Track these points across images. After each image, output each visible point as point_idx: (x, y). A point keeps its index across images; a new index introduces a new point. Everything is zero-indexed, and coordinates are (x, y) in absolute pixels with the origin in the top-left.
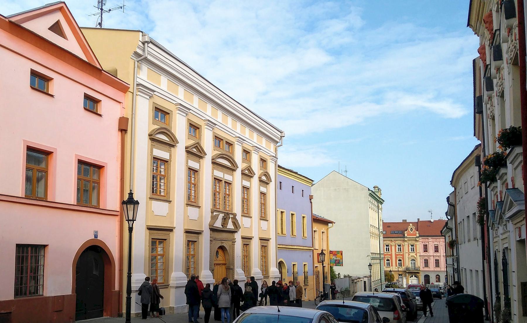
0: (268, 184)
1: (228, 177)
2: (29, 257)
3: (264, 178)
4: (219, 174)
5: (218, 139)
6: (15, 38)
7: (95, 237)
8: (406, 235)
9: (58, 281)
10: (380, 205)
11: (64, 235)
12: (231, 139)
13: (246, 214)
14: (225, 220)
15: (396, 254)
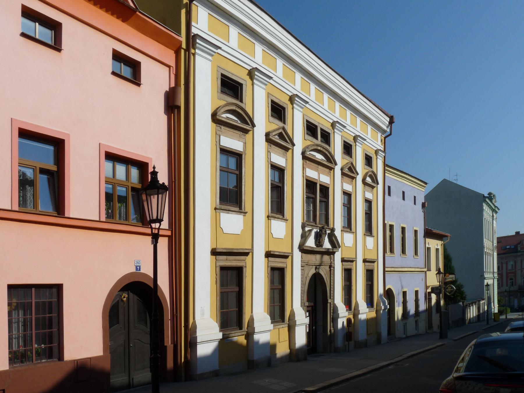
0: (373, 187)
1: (324, 179)
2: (39, 309)
3: (368, 180)
4: (312, 174)
5: (311, 129)
6: (244, 311)
7: (137, 269)
8: (519, 249)
9: (84, 338)
10: (494, 215)
11: (90, 268)
12: (327, 127)
13: (348, 226)
14: (319, 238)
15: (507, 272)
